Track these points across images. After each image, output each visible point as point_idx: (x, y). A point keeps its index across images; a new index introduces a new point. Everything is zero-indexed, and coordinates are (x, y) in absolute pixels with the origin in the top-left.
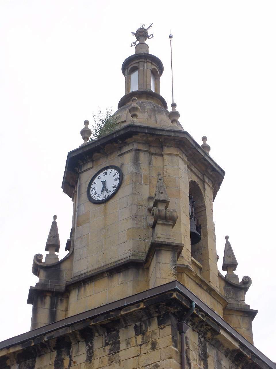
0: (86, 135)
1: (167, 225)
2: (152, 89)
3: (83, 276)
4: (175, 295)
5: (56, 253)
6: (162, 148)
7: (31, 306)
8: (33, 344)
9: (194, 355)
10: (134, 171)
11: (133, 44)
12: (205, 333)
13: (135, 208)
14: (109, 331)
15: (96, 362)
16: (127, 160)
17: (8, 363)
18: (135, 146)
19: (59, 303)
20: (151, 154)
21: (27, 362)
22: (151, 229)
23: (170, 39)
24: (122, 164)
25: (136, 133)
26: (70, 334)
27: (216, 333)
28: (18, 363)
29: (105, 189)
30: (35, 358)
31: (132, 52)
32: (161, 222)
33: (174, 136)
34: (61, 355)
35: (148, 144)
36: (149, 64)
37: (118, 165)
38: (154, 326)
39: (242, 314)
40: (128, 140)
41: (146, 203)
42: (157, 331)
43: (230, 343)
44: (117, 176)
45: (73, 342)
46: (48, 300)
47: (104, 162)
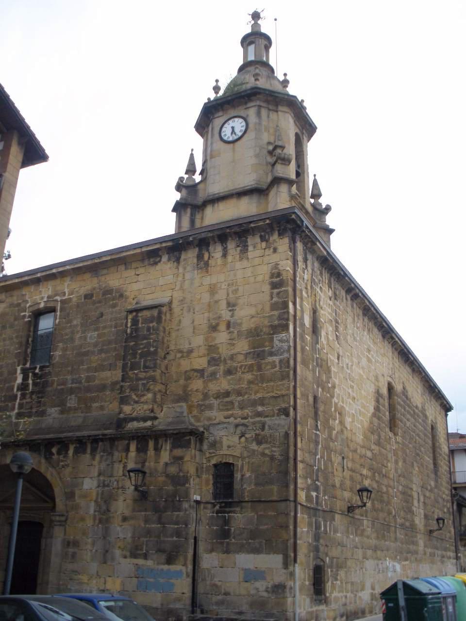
0: (217, 90)
1: (284, 164)
2: (265, 59)
3: (217, 195)
4: (293, 216)
5: (193, 177)
6: (277, 106)
7: (175, 214)
8: (181, 242)
9: (300, 258)
10: (257, 121)
11: (249, 23)
12: (307, 244)
13: (258, 149)
14: (240, 237)
15: (230, 258)
16: (252, 113)
17: (160, 253)
18: (258, 103)
19: (197, 213)
20: (269, 110)
21: (175, 253)
22: (270, 167)
23: (275, 22)
24: (248, 116)
25: (259, 93)
26: (210, 237)
27: (314, 244)
28: (167, 253)
29: (233, 132)
30: (181, 251)
31: (249, 30)
32: (280, 162)
33: (287, 99)
34: (202, 251)
35: (267, 101)
36: (263, 40)
37: (244, 116)
38: (275, 236)
39: (324, 231)
40: (253, 98)
41: (266, 147)
42: (277, 240)
43: (321, 251)
44: (244, 124)
45: (211, 243)
46: (189, 211)
47: (232, 113)
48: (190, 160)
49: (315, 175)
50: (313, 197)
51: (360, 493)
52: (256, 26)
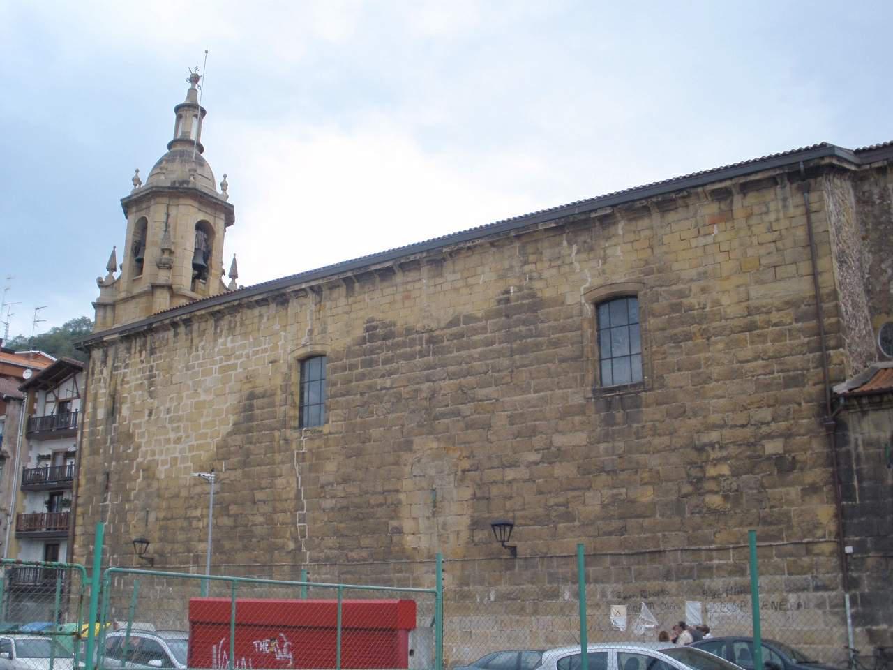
52: (192, 92)
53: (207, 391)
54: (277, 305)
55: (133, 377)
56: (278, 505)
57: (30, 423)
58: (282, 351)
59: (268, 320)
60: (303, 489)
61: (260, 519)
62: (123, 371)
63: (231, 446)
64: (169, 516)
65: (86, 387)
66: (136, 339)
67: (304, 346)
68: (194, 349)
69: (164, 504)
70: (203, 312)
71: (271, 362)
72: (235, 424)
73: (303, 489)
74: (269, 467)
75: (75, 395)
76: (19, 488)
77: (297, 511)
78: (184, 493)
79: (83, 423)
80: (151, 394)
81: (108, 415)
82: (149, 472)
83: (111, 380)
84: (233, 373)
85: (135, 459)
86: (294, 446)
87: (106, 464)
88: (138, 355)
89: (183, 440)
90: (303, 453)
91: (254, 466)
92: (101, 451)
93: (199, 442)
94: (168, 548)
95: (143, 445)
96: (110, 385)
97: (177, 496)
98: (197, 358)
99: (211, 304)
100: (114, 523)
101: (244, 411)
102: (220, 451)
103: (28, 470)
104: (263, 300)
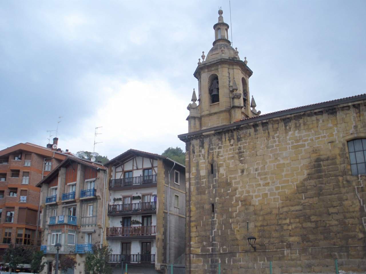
7: (187, 121)
48: (193, 95)
49: (252, 96)
50: (252, 106)
51: (250, 240)
52: (221, 18)
53: (283, 158)
54: (328, 114)
55: (225, 153)
56: (348, 215)
57: (110, 182)
58: (337, 137)
59: (323, 121)
60: (364, 206)
61: (335, 222)
62: (217, 150)
63: (308, 186)
64: (265, 224)
65: (190, 159)
66: (225, 134)
67: (352, 134)
68: (271, 137)
69: (261, 218)
70: (278, 118)
71: (330, 142)
72: (308, 174)
73: (364, 206)
74: (337, 195)
75: (135, 168)
76: (107, 214)
77: (362, 217)
78: (275, 211)
79: (190, 178)
80: (241, 161)
81: (209, 173)
82: (246, 202)
83: (208, 155)
84: (303, 149)
85: (235, 196)
86: (354, 184)
87: (211, 199)
88: (228, 142)
89: (270, 184)
90: (362, 187)
91: (326, 195)
92: (206, 192)
93: (283, 185)
94: (266, 241)
95: (239, 188)
96: (208, 158)
97: (270, 213)
98: (275, 142)
99: (285, 114)
100: (221, 230)
101: (315, 168)
102: (300, 189)
103: (111, 206)
104: (319, 112)
